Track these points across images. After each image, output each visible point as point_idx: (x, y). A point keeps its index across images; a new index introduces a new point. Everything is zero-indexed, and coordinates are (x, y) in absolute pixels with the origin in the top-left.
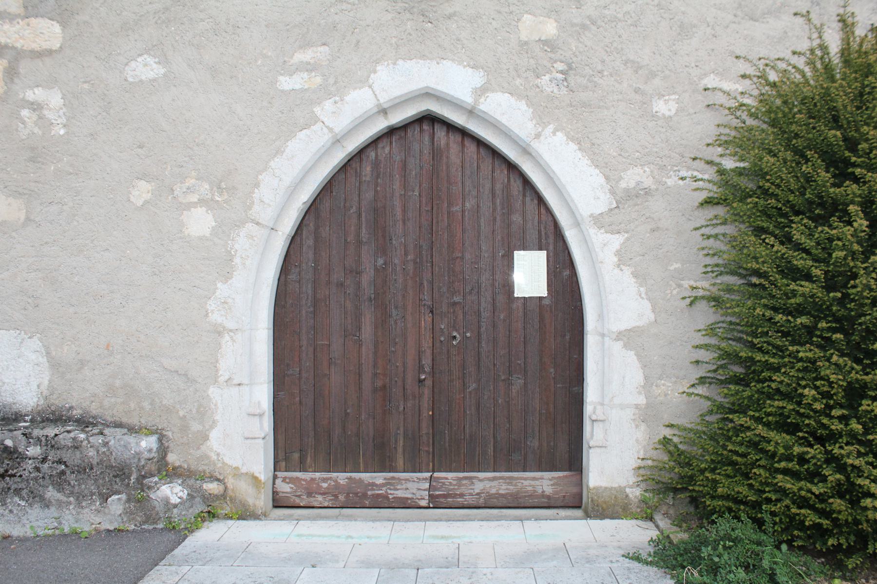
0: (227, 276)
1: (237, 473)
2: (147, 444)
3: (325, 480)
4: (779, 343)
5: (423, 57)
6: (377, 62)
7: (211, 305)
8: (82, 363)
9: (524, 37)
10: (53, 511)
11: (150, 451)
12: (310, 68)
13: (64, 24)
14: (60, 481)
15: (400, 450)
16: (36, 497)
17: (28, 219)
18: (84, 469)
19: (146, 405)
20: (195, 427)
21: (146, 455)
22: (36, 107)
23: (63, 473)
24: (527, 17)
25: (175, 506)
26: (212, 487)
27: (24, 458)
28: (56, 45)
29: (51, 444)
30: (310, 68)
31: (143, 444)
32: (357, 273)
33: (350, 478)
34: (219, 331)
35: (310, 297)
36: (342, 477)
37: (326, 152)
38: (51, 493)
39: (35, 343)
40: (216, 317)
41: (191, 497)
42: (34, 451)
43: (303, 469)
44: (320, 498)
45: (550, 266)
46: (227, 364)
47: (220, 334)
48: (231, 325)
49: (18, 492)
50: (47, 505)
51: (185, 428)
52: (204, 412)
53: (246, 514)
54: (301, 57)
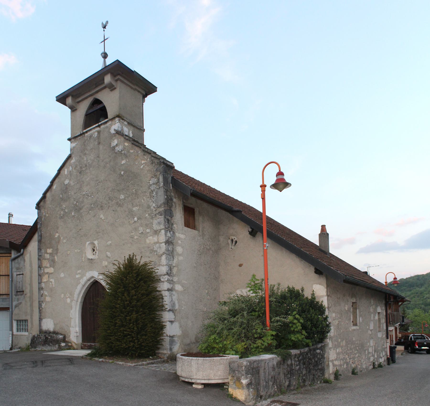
0: (72, 309)
1: (73, 342)
2: (61, 337)
3: (87, 344)
4: (118, 343)
6: (86, 272)
8: (57, 324)
9: (103, 265)
10: (51, 347)
12: (79, 273)
13: (54, 268)
14: (51, 342)
16: (49, 345)
17: (51, 301)
18: (54, 341)
20: (69, 334)
22: (51, 282)
23: (52, 341)
24: (104, 262)
26: (70, 344)
27: (48, 338)
28: (53, 272)
29: (51, 337)
30: (79, 273)
34: (71, 318)
35: (136, 364)
36: (89, 344)
37: (82, 288)
38: (51, 344)
39: (52, 321)
41: (66, 345)
43: (85, 343)
45: (66, 92)
47: (71, 319)
50: (50, 346)
51: (68, 335)
52: (70, 332)
53: (74, 349)
54: (78, 272)
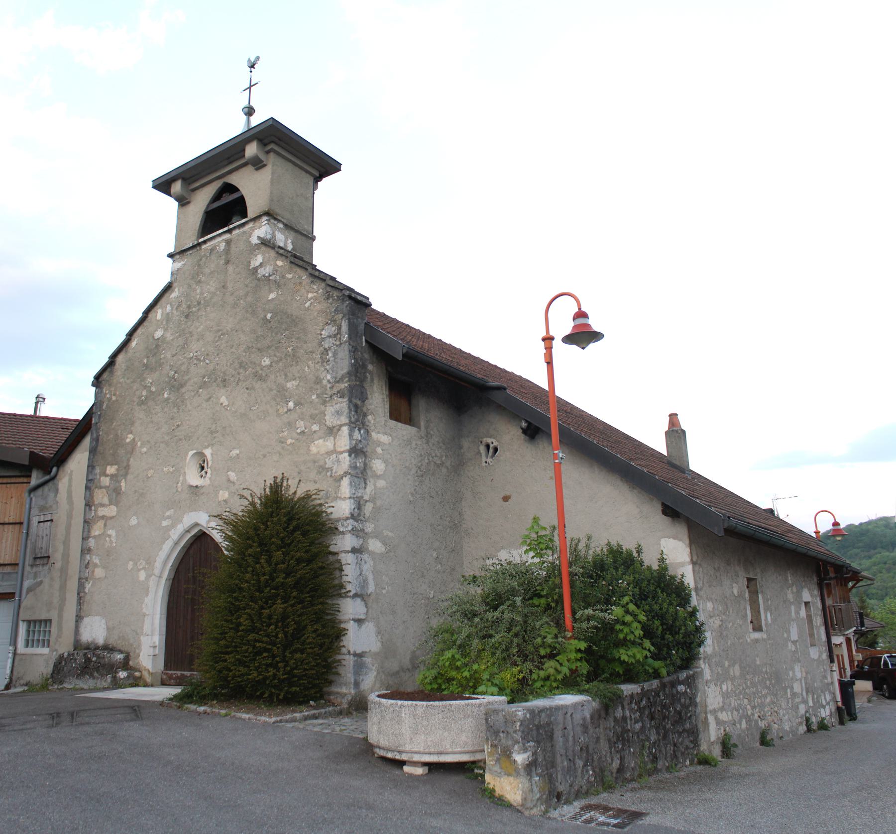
0: (147, 595)
3: (175, 674)
5: (195, 511)
7: (144, 606)
10: (95, 681)
11: (120, 659)
13: (117, 507)
15: (846, 714)
18: (103, 666)
19: (127, 643)
20: (137, 651)
21: (119, 660)
23: (99, 667)
25: (122, 679)
26: (137, 674)
30: (169, 517)
31: (119, 657)
32: (691, 616)
33: (181, 674)
36: (179, 673)
38: (96, 674)
40: (144, 610)
42: (94, 659)
44: (172, 681)
46: (147, 627)
48: (147, 613)
49: (88, 673)
50: (94, 678)
51: (135, 652)
